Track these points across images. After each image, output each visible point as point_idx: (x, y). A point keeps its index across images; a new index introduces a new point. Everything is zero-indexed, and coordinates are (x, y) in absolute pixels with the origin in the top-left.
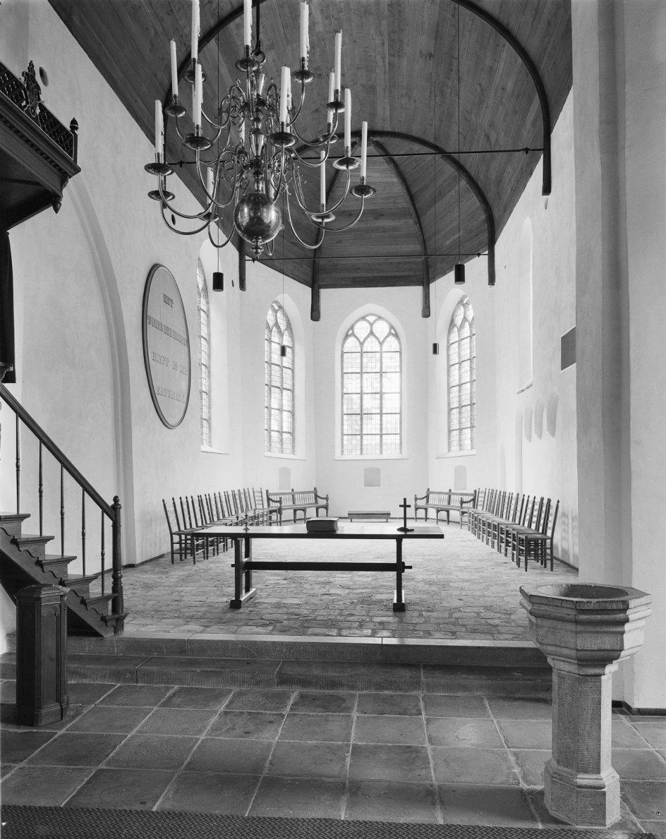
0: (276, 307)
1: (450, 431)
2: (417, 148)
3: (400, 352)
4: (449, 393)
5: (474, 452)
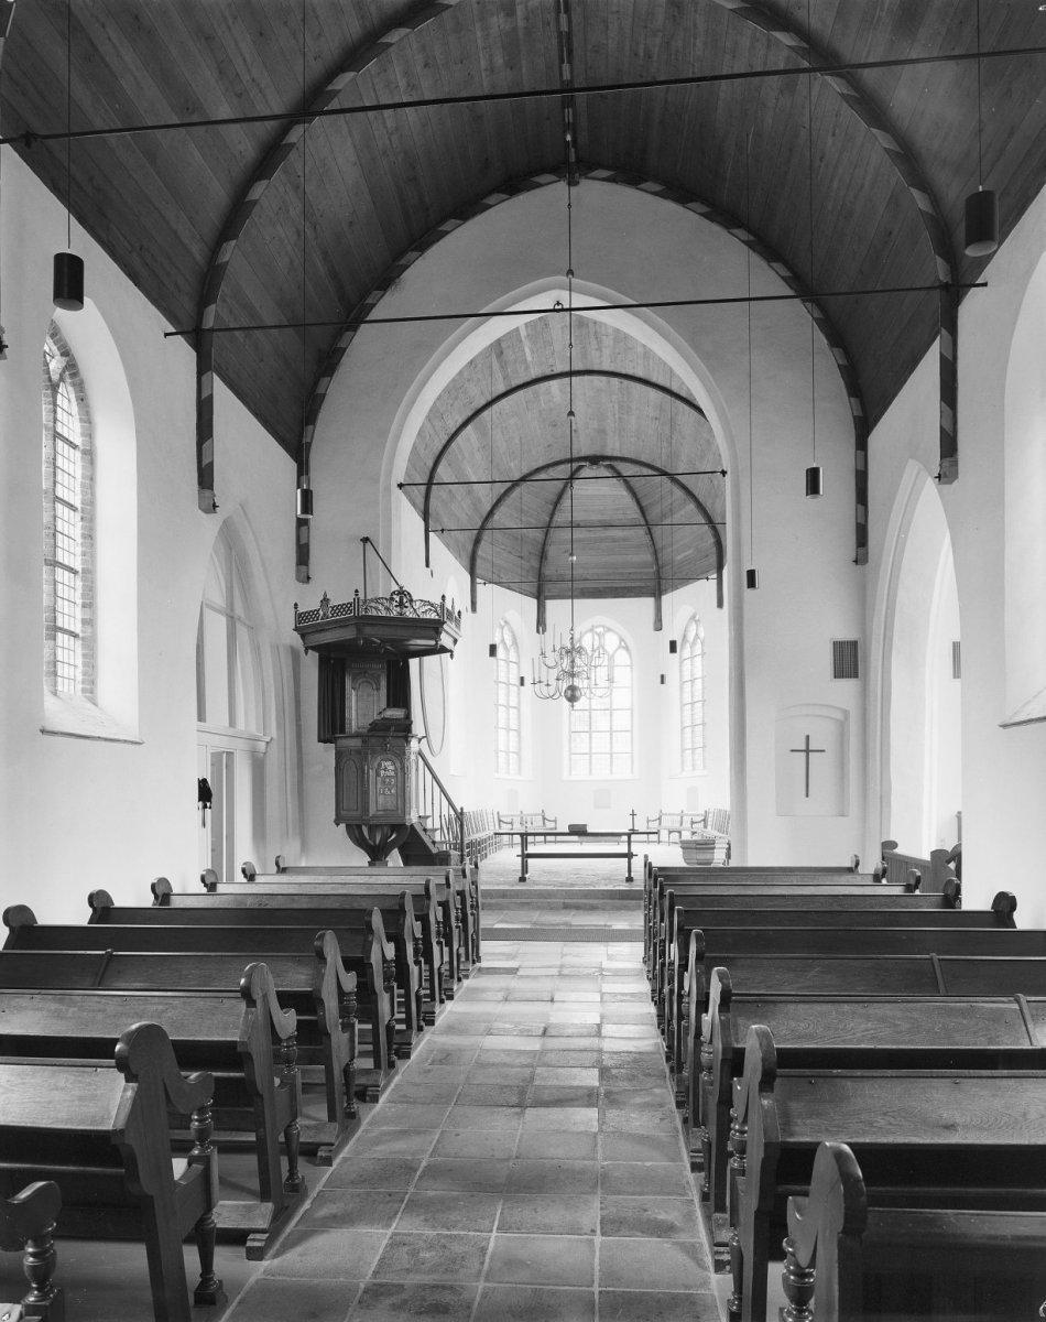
0: (503, 623)
1: (683, 751)
2: (646, 471)
3: (631, 666)
4: (681, 689)
5: (705, 772)
